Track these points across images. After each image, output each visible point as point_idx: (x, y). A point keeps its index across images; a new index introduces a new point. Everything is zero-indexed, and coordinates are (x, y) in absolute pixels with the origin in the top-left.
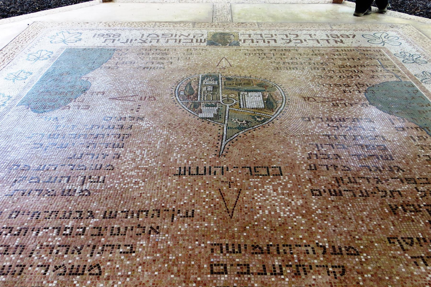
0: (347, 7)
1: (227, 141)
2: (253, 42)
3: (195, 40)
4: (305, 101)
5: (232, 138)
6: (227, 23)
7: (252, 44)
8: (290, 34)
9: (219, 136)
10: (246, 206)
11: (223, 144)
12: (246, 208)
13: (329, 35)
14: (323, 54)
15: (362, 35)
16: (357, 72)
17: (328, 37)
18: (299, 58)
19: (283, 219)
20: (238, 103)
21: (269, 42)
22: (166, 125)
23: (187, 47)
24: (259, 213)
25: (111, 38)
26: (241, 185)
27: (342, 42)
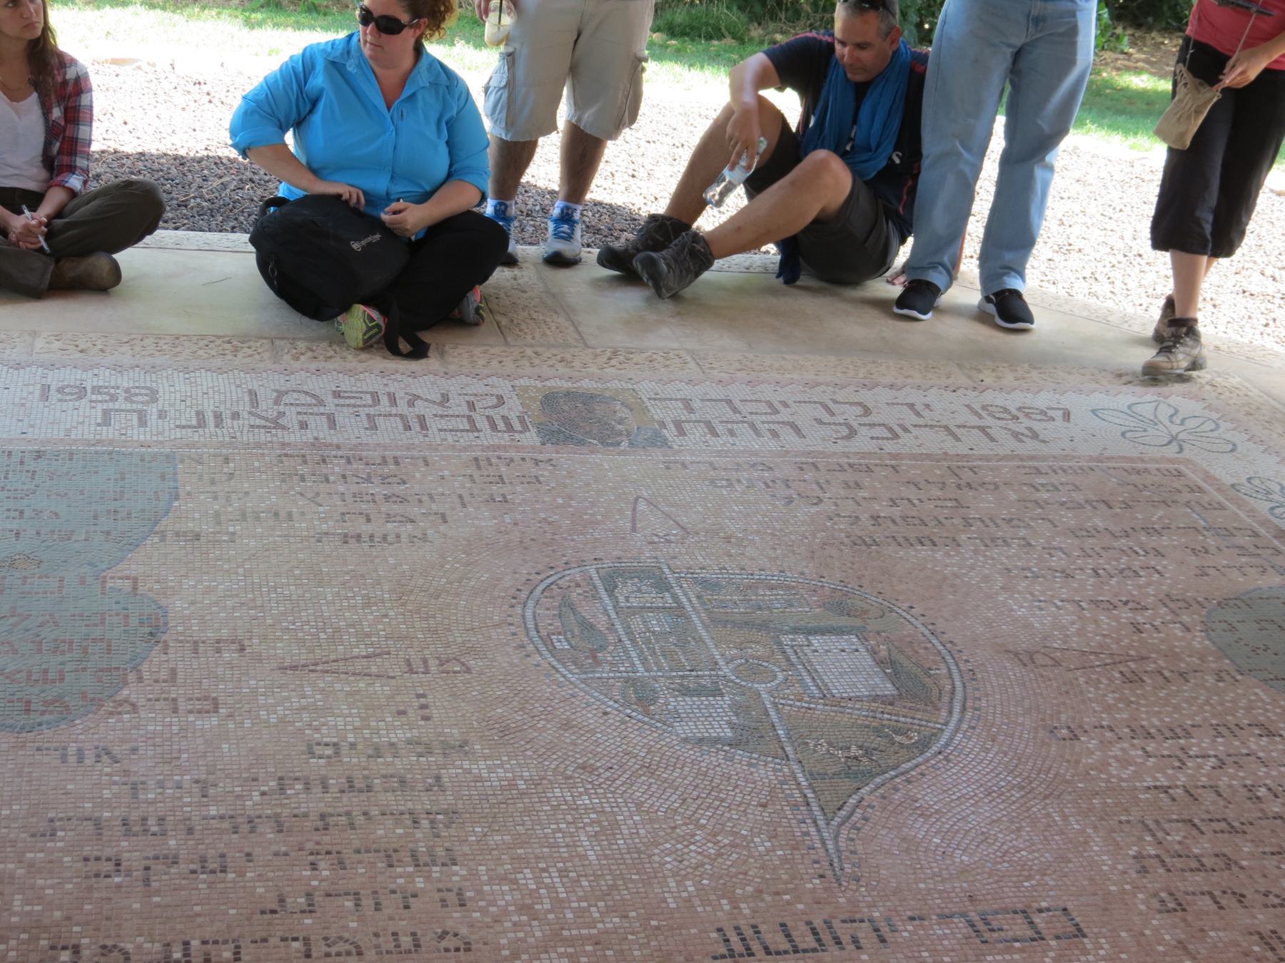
8: (835, 402)
13: (977, 407)
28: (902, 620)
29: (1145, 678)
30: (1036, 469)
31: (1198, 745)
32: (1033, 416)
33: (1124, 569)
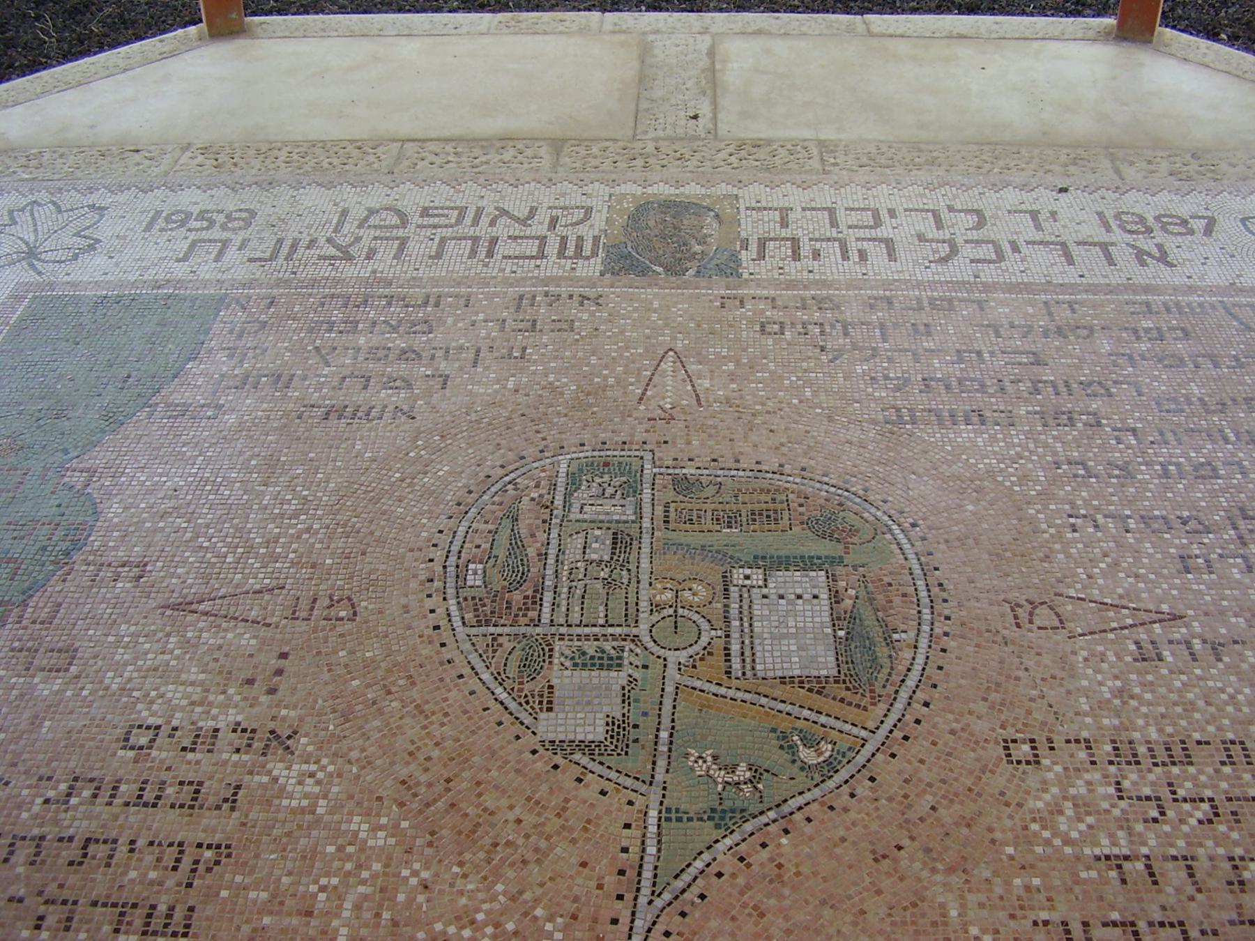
0: (1172, 62)
1: (659, 903)
2: (796, 256)
3: (552, 247)
5: (679, 884)
6: (695, 145)
7: (792, 268)
8: (951, 209)
9: (622, 872)
11: (638, 923)
13: (1109, 215)
14: (1091, 330)
15: (1243, 221)
16: (1232, 437)
20: (719, 644)
21: (863, 255)
22: (388, 789)
23: (518, 283)
25: (216, 233)
27: (1163, 258)
28: (894, 547)
29: (1166, 653)
30: (1148, 305)
31: (1194, 778)
32: (1171, 228)
33: (1202, 464)
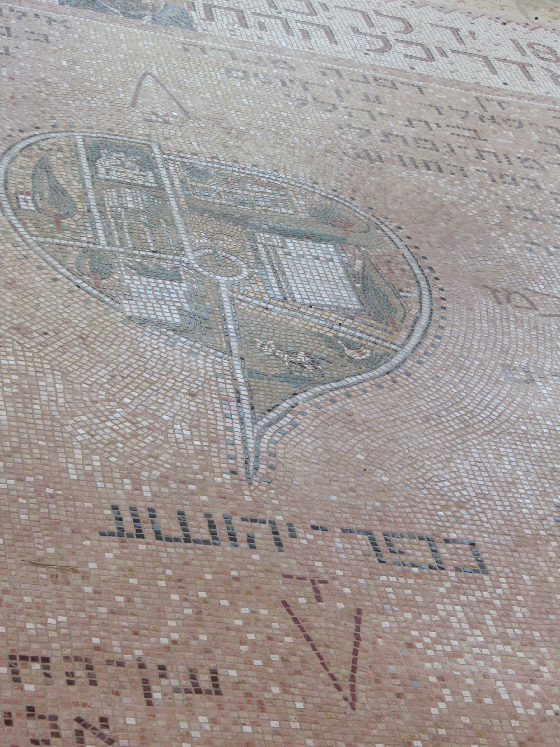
4: (500, 303)
10: (392, 669)
12: (394, 676)
13: (523, 43)
17: (523, 53)
18: (438, 125)
19: (526, 725)
24: (442, 700)
26: (357, 592)
